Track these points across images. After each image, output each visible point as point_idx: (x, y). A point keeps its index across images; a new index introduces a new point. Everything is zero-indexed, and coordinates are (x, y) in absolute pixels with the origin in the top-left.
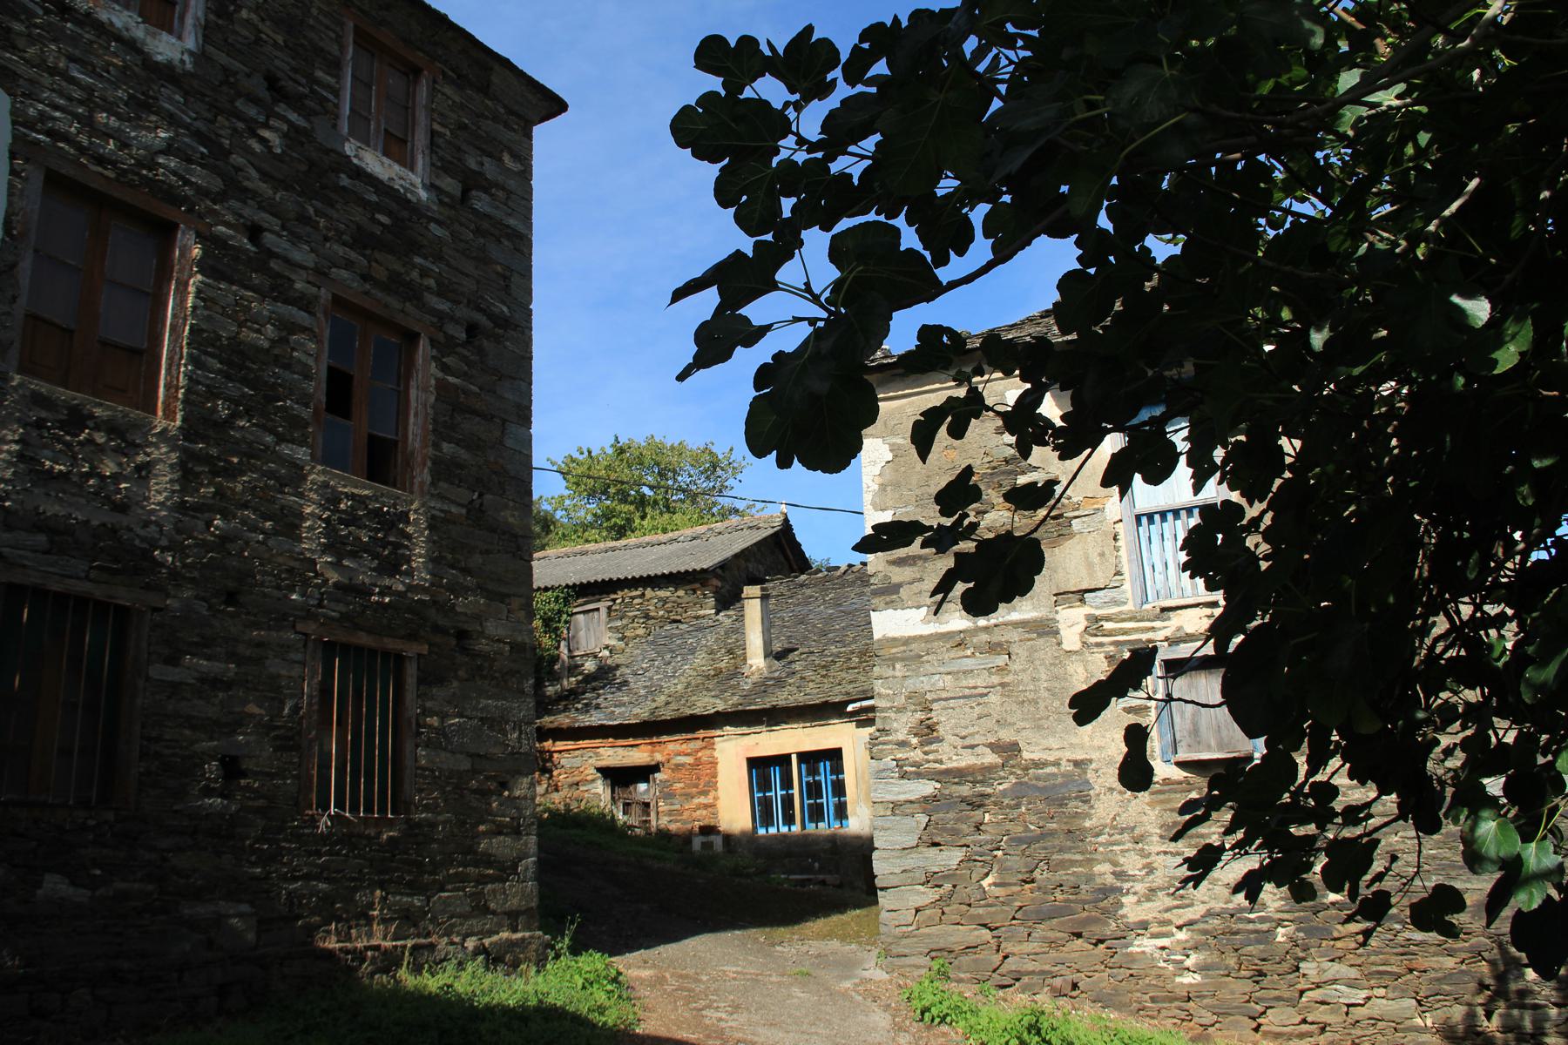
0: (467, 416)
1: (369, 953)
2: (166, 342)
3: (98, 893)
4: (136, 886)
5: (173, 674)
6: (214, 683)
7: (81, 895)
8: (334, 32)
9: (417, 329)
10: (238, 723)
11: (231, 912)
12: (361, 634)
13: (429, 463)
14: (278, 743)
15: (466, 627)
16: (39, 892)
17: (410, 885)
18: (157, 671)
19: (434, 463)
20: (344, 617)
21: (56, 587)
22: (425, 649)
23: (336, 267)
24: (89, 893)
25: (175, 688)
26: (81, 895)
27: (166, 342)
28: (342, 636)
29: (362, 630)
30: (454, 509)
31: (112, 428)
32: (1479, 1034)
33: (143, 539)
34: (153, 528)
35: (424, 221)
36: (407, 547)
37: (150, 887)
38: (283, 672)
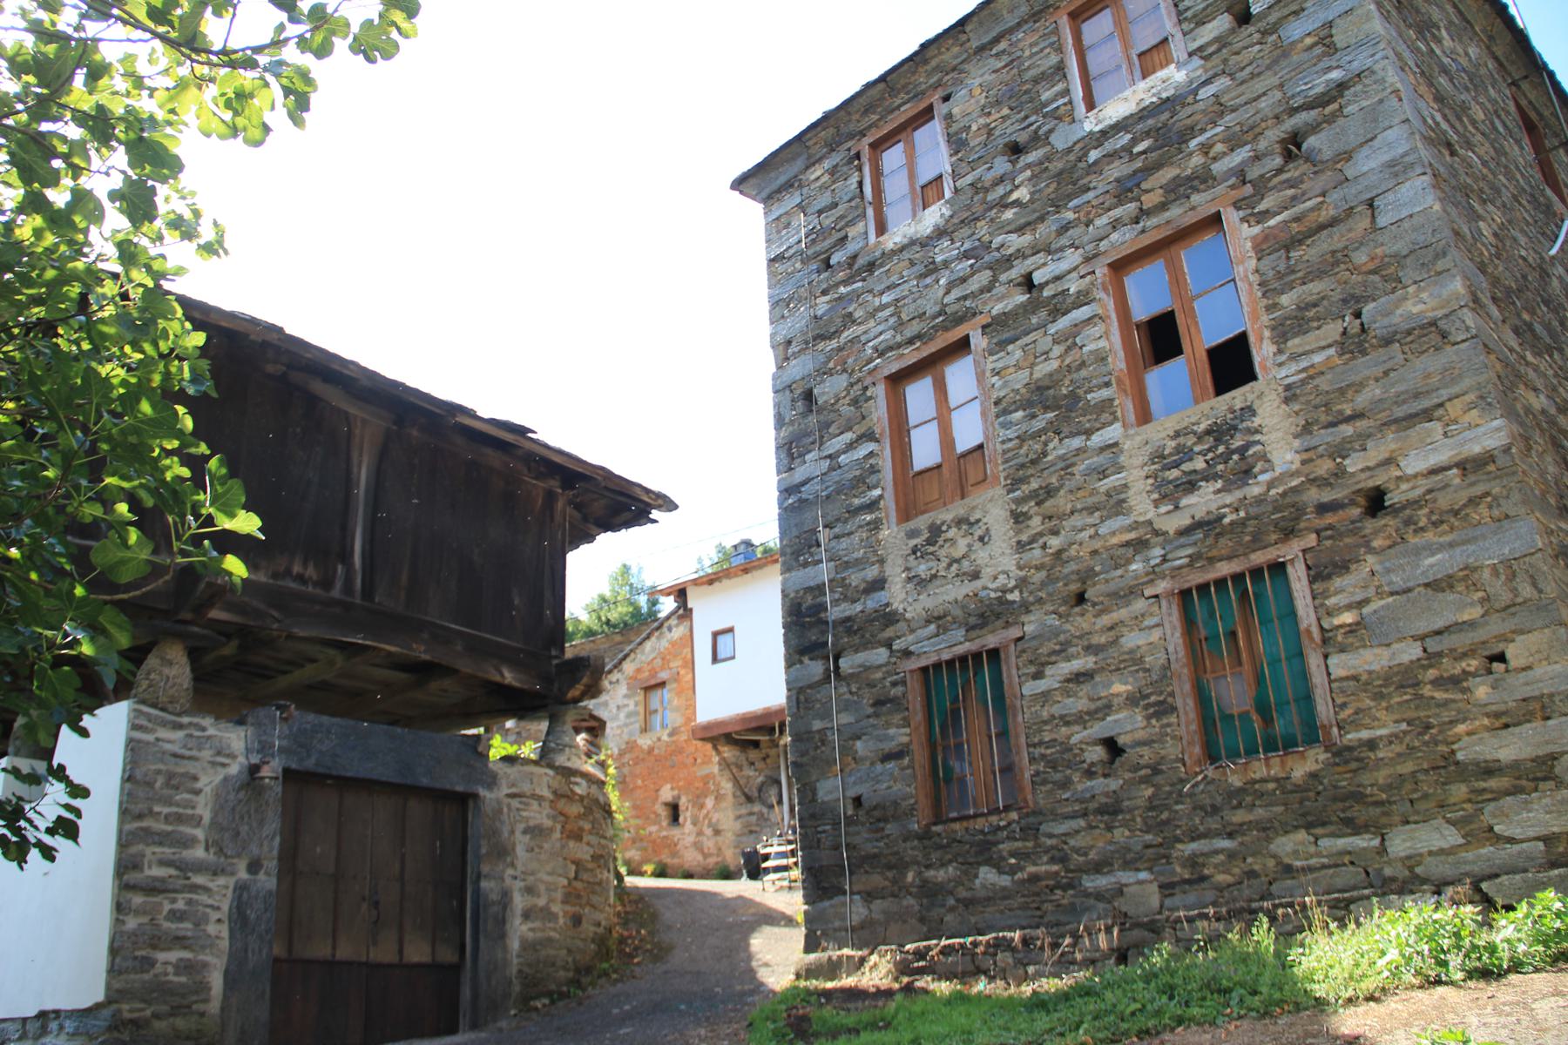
0: (1309, 242)
1: (1280, 911)
2: (488, 636)
3: (1016, 877)
4: (1043, 868)
5: (1042, 685)
6: (1080, 677)
7: (1005, 881)
8: (1045, 48)
9: (1213, 211)
10: (1105, 709)
11: (1131, 880)
12: (1219, 565)
13: (1267, 333)
14: (1151, 710)
15: (1371, 484)
16: (977, 882)
17: (1348, 822)
18: (1031, 687)
19: (1273, 329)
20: (1193, 558)
21: (946, 656)
22: (1311, 540)
23: (1101, 240)
24: (1009, 878)
25: (1045, 696)
26: (1005, 881)
27: (488, 636)
28: (1196, 578)
29: (1221, 560)
30: (1317, 358)
31: (959, 522)
32: (1337, 1038)
33: (995, 591)
34: (1001, 577)
35: (1190, 99)
36: (1258, 442)
37: (1055, 868)
38: (1140, 643)
